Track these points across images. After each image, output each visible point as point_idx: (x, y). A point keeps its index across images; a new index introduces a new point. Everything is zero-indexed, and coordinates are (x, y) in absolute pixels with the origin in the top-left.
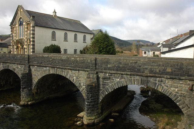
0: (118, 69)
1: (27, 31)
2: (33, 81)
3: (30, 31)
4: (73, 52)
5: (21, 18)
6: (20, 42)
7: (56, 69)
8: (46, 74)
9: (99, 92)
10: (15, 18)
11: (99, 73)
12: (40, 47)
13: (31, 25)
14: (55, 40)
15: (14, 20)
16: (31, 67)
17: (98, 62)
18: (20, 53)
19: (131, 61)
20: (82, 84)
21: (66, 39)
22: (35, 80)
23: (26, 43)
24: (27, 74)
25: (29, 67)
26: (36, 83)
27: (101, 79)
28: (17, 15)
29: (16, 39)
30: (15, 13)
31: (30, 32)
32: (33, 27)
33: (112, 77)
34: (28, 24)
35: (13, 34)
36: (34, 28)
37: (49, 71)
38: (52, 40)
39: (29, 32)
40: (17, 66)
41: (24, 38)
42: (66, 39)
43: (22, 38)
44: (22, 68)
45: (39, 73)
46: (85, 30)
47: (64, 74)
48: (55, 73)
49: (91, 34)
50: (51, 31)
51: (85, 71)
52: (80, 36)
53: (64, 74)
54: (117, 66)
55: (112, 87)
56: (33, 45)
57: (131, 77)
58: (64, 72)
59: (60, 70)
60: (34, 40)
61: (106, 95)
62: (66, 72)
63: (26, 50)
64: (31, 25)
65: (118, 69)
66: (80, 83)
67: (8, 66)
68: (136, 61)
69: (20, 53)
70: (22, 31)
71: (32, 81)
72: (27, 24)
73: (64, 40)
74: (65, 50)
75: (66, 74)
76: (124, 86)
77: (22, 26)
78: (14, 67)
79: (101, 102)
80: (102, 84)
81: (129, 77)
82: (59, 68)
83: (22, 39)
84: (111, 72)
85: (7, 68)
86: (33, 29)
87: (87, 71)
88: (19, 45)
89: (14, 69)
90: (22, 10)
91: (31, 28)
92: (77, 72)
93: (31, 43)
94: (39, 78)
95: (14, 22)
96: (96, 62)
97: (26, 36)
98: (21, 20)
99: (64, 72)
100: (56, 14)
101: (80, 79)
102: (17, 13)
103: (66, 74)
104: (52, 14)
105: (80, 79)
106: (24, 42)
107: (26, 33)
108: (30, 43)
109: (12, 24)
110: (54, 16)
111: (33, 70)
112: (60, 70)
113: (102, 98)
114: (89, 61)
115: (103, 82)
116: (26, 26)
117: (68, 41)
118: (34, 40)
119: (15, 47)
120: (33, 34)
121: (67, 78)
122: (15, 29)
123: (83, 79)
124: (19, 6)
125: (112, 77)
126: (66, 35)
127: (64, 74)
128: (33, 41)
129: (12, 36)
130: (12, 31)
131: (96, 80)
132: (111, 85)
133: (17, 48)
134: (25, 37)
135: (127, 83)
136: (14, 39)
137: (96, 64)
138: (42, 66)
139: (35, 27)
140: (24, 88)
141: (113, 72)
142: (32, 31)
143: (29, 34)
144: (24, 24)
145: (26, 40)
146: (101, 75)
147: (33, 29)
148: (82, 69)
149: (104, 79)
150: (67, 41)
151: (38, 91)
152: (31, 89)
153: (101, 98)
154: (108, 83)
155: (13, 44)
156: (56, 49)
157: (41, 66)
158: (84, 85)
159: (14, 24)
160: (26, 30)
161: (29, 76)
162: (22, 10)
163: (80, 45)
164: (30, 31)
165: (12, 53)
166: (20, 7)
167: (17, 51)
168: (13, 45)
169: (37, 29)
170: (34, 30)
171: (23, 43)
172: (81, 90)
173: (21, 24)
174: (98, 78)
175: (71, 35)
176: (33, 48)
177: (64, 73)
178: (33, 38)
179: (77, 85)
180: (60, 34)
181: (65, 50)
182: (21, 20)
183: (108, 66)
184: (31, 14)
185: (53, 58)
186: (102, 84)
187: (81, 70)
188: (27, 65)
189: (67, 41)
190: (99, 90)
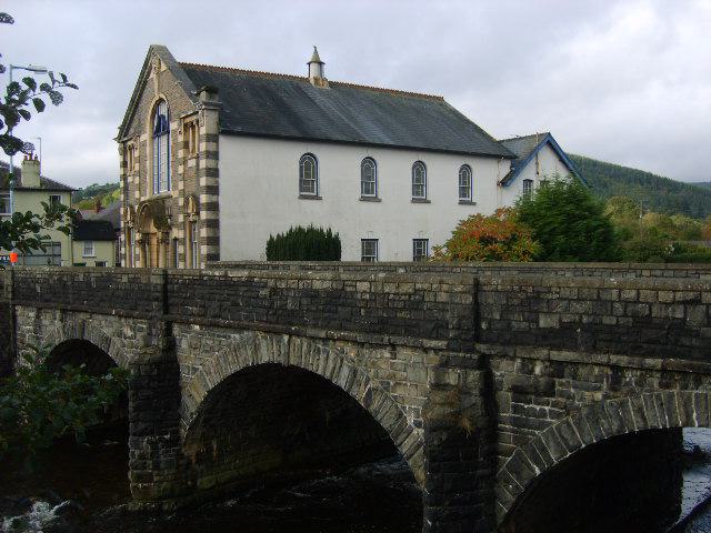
0: (598, 336)
1: (185, 162)
2: (185, 398)
3: (198, 157)
4: (407, 255)
5: (161, 100)
6: (156, 212)
7: (286, 338)
8: (242, 366)
9: (495, 464)
10: (138, 104)
11: (494, 362)
12: (245, 240)
13: (203, 131)
14: (317, 198)
15: (133, 115)
16: (176, 330)
17: (489, 299)
18: (155, 263)
19: (664, 296)
20: (411, 420)
21: (369, 189)
22: (194, 393)
23: (181, 218)
24: (156, 364)
25: (168, 332)
26: (199, 412)
27: (505, 396)
28: (144, 88)
29: (143, 199)
30: (139, 82)
31: (198, 165)
32: (212, 138)
33: (561, 384)
34: (190, 127)
35: (130, 179)
36: (217, 141)
37: (256, 348)
38: (302, 197)
39: (192, 163)
40: (116, 325)
41: (174, 194)
42: (369, 189)
43: (163, 191)
44: (139, 335)
45: (210, 360)
46: (463, 141)
47: (325, 368)
48: (282, 360)
49: (497, 157)
50: (298, 151)
51: (426, 350)
52: (444, 172)
53: (321, 365)
54: (585, 320)
55: (563, 438)
56: (214, 224)
57: (667, 386)
58: (323, 356)
59: (305, 348)
60: (214, 198)
61: (537, 486)
62: (332, 356)
63: (181, 249)
64: (203, 131)
65: (598, 336)
66: (400, 415)
67: (83, 326)
68: (691, 295)
69: (155, 263)
70: (164, 159)
71: (179, 398)
72: (186, 125)
73: (358, 194)
74: (419, 245)
75: (331, 365)
76: (632, 433)
77: (164, 139)
78: (105, 330)
79: (508, 516)
80: (515, 422)
81: (656, 385)
82: (298, 335)
83: (164, 199)
84: (555, 355)
85: (77, 336)
86: (212, 147)
87: (436, 350)
88: (153, 229)
89: (108, 340)
90: (164, 68)
91: (203, 147)
92: (387, 355)
93: (204, 215)
94: (211, 386)
95: (135, 124)
96: (475, 297)
97: (181, 185)
98: (163, 110)
99: (323, 356)
100: (321, 71)
101: (400, 392)
102: (145, 82)
103: (331, 365)
104: (302, 71)
105: (400, 392)
106: (175, 211)
107: (181, 169)
108: (198, 214)
109: (126, 134)
110: (312, 81)
111: (184, 345)
112: (305, 348)
113: (511, 498)
114: (443, 297)
115: (516, 409)
116: (181, 139)
117: (320, 199)
118: (214, 198)
119: (138, 236)
120: (213, 173)
121: (339, 388)
122: (136, 154)
123: (413, 392)
124: (152, 49)
125: (561, 384)
126: (368, 168)
127: (325, 368)
128: (213, 207)
129: (126, 189)
130: (124, 164)
131: (476, 398)
132: (558, 428)
133: (144, 242)
134: (175, 187)
135: (644, 419)
136: (131, 201)
137: (477, 318)
138: (229, 327)
139: (222, 139)
140: (142, 434)
141: (566, 355)
142: (207, 157)
143: (192, 173)
144: (173, 126)
145: (181, 202)
146: (506, 371)
147: (212, 147)
148: (411, 341)
149: (519, 392)
150: (376, 200)
151: (210, 450)
152: (175, 440)
153: (507, 496)
154: (543, 414)
155: (131, 225)
156: (316, 246)
157: (218, 326)
158: (418, 425)
159: (132, 131)
160: (181, 154)
161: (164, 371)
162: (164, 68)
163: (441, 220)
164: (198, 157)
165: (123, 265)
166: (157, 53)
167: (145, 257)
168: (129, 229)
169: (230, 148)
170: (213, 155)
171: (170, 216)
172: (404, 449)
173: (161, 129)
174: (489, 387)
175: (394, 170)
176: (214, 241)
177: (322, 362)
178: (213, 190)
179: (387, 422)
180: (339, 167)
181: (419, 245)
182: (163, 110)
183: (542, 324)
184: (203, 80)
185: (271, 283)
186: (515, 422)
187: (404, 346)
188: (161, 325)
189: (376, 200)
190: (493, 456)
